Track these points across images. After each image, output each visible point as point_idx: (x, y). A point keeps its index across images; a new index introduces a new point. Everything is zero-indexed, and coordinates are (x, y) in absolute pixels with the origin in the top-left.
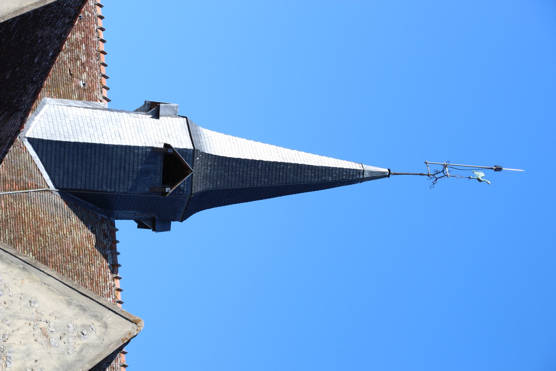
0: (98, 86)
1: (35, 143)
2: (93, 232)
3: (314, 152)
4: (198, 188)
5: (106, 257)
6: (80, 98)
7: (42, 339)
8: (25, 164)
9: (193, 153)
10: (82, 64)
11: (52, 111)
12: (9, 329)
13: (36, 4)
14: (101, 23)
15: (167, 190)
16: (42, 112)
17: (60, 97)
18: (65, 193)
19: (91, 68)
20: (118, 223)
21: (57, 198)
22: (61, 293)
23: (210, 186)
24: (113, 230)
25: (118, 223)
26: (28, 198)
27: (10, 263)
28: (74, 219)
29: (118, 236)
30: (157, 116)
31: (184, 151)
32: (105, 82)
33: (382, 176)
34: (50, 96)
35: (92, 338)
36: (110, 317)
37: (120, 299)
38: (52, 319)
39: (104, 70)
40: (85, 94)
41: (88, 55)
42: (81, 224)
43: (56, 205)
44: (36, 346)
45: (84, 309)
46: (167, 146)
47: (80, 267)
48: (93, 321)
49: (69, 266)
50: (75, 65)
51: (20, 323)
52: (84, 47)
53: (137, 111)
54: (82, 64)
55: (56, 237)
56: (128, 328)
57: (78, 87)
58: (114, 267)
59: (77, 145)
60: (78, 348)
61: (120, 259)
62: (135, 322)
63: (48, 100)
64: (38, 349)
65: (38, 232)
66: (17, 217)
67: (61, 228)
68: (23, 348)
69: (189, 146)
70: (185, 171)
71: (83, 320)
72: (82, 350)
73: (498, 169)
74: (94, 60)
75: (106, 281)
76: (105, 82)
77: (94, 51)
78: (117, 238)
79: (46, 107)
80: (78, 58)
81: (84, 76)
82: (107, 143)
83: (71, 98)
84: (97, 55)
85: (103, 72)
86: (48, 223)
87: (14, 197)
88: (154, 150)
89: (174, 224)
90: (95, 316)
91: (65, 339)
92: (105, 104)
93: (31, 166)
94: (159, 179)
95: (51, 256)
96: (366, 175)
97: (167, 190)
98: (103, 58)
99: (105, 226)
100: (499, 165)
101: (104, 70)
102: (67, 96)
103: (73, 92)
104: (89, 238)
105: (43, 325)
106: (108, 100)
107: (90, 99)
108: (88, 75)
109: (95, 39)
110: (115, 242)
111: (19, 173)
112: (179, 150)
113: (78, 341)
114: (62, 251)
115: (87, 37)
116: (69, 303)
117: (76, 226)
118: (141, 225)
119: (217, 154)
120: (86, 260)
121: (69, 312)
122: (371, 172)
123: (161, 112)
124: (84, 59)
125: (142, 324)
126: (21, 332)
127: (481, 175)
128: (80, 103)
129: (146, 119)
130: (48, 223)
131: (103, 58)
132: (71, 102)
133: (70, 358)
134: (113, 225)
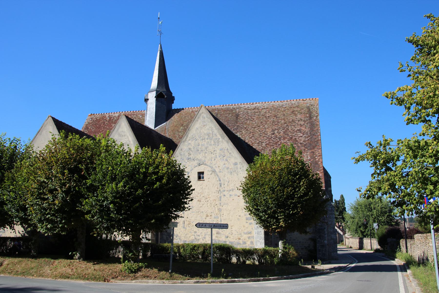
0: (141, 112)
1: (155, 127)
2: (175, 114)
3: (155, 62)
4: (165, 90)
5: (181, 111)
6: (144, 117)
7: (205, 126)
8: (160, 129)
9: (157, 92)
10: (136, 116)
11: (148, 123)
12: (203, 133)
13: (235, 149)
14: (126, 112)
15: (165, 97)
16: (148, 125)
17: (144, 121)
18: (167, 120)
19: (137, 114)
20: (173, 108)
21: (168, 122)
22: (195, 122)
23: (164, 87)
24: (175, 109)
25: (173, 108)
26: (168, 128)
27: (189, 134)
28: (172, 118)
29: (176, 108)
30: (148, 99)
31: (156, 93)
32: (140, 111)
33: (161, 46)
34: (144, 123)
35: (205, 116)
36: (201, 112)
37: (190, 108)
38: (201, 124)
39: (137, 111)
40: (143, 115)
41: (134, 115)
42: (174, 116)
43: (170, 122)
44: (206, 128)
45: (199, 118)
46: (155, 97)
47: (183, 117)
48: (201, 116)
49: (183, 119)
50: (136, 118)
51: (202, 131)
52: (132, 116)
53: (147, 103)
54: (136, 116)
55: (177, 122)
56: (203, 108)
57: (142, 117)
58: (183, 109)
59: (156, 118)
60: (207, 119)
61: (181, 108)
62: (202, 106)
63: (145, 124)
64: (207, 127)
65: (176, 126)
66: (172, 131)
67: (175, 121)
68: (207, 130)
69: (155, 92)
70: (161, 93)
71: (201, 118)
72: (208, 118)
73: (159, 18)
74: (135, 113)
75: (187, 111)
76: (140, 111)
77: (133, 113)
78: (179, 108)
79: (147, 124)
80: (135, 117)
81: (139, 116)
82: (155, 111)
83: (144, 119)
84: (134, 113)
85: (138, 111)
86: (174, 124)
87: (168, 131)
88: (156, 100)
89: (173, 95)
90: (200, 115)
91: (205, 122)
92: (145, 111)
93: (161, 128)
94: (163, 99)
95: (181, 123)
96: (161, 50)
97: (165, 97)
98: (135, 111)
99: (174, 111)
100: (158, 18)
101: (137, 111)
102: (144, 120)
103: (143, 118)
104: (177, 115)
105: (202, 126)
106: (144, 110)
107: (144, 115)
108: (139, 115)
109: (130, 113)
110: (177, 109)
111: (162, 130)
112: (156, 94)
113: (206, 119)
114: (180, 121)
115: (130, 115)
116: (197, 121)
117: (174, 118)
118: (173, 103)
119: (157, 85)
120: (182, 115)
121: (199, 121)
122: (160, 48)
123: (147, 98)
124: (135, 116)
125: (202, 105)
126: (204, 131)
127: (160, 22)
128: (145, 117)
129: (149, 102)
130: (174, 124)
131: (135, 111)
132: (145, 119)
133: (209, 120)
134: (173, 109)
